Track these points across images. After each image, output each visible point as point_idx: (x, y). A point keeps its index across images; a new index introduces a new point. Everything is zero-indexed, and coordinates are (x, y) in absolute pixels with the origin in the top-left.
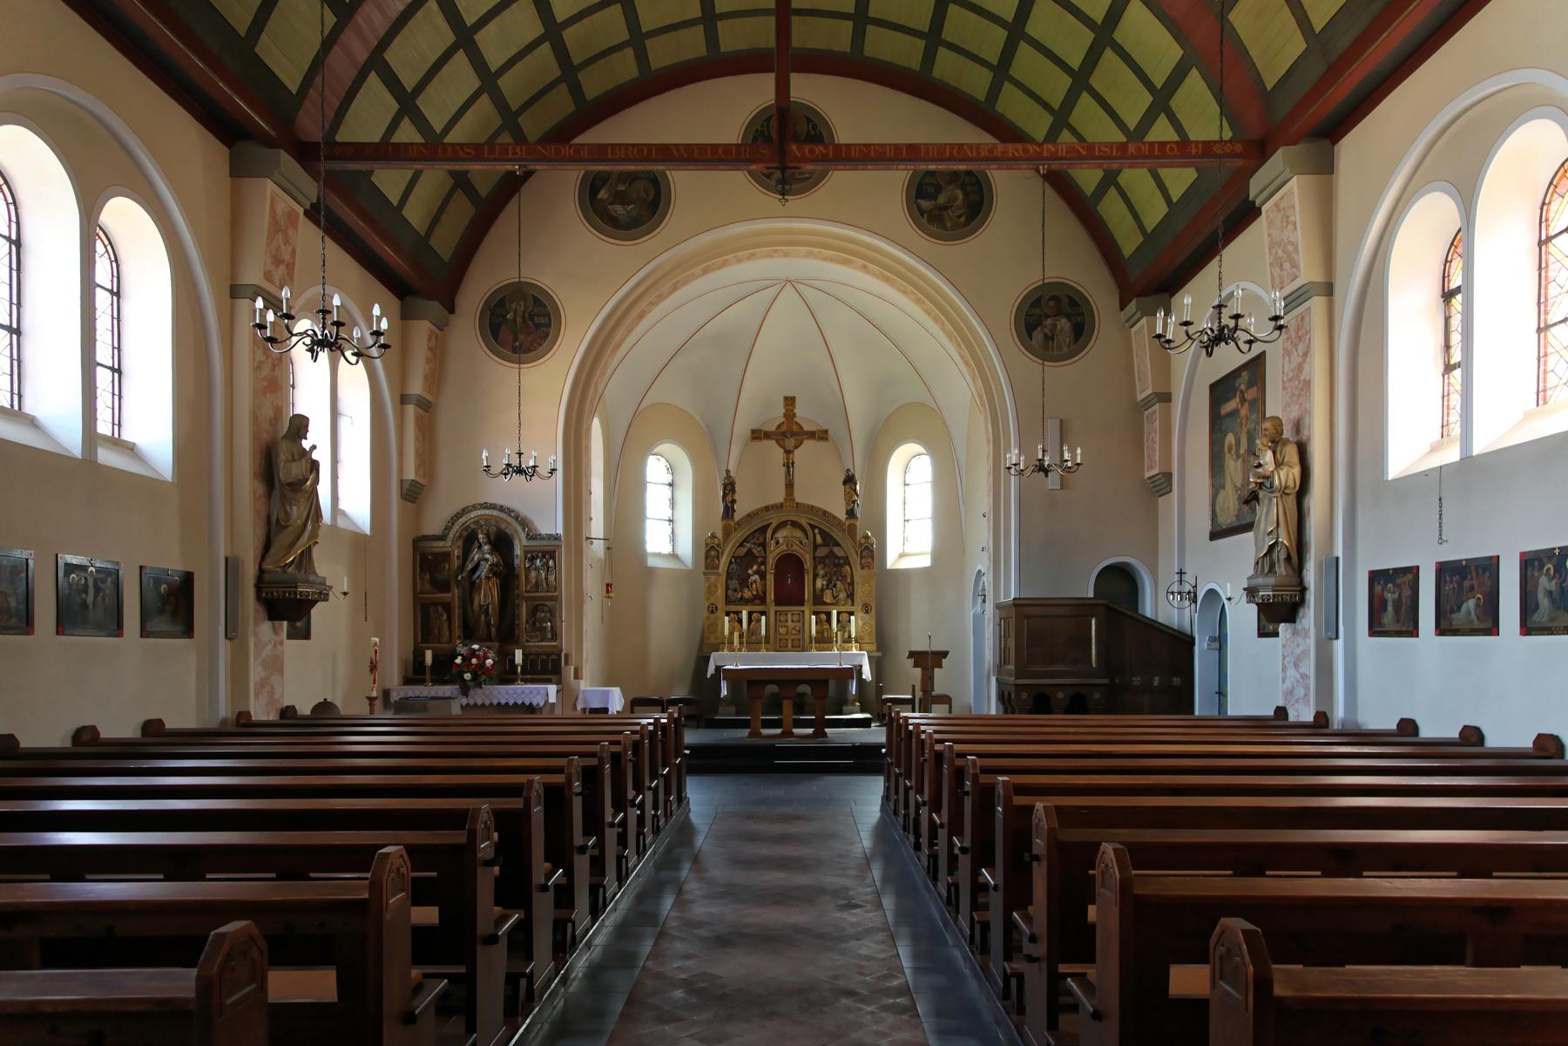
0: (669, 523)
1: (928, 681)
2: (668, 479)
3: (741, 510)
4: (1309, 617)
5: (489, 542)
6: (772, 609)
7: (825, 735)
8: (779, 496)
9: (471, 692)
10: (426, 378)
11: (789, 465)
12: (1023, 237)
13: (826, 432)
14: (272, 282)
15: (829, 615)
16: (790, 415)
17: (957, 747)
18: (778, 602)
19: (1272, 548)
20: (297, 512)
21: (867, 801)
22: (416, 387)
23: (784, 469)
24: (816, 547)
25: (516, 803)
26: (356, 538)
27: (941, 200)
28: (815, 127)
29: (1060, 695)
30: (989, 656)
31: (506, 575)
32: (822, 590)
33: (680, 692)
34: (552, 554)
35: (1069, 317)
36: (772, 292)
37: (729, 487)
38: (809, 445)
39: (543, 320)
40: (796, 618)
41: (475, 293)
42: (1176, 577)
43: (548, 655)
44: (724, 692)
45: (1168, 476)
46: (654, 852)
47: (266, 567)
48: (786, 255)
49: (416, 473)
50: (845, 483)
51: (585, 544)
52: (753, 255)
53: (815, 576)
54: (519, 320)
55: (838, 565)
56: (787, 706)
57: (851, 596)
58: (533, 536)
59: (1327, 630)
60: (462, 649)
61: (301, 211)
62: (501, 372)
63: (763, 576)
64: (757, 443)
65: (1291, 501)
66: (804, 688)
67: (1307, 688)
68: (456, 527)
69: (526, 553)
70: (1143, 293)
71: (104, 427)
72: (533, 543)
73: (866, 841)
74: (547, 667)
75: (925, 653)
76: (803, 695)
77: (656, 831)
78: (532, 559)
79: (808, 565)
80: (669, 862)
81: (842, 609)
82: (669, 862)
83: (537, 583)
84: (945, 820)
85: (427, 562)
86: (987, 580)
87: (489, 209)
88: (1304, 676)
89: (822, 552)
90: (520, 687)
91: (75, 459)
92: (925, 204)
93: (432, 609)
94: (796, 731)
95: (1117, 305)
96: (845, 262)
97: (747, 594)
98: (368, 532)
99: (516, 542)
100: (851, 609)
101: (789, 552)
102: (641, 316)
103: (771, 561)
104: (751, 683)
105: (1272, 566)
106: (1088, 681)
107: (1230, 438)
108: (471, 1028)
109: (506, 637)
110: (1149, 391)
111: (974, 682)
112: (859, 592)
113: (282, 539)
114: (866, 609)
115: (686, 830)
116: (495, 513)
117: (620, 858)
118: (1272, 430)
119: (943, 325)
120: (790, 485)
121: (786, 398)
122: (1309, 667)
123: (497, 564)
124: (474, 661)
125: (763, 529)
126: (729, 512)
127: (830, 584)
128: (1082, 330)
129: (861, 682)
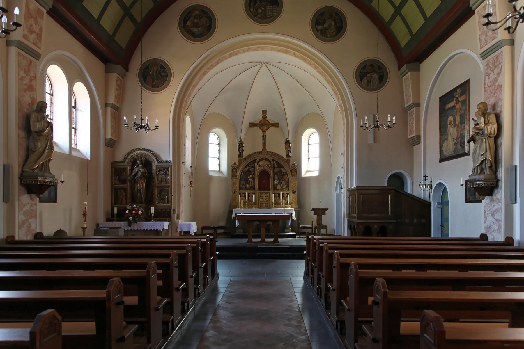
0: (218, 158)
1: (320, 220)
2: (218, 142)
3: (246, 154)
4: (501, 194)
5: (142, 163)
6: (258, 192)
7: (278, 242)
8: (260, 148)
9: (133, 225)
10: (116, 97)
11: (264, 136)
12: (359, 42)
13: (278, 124)
14: (29, 41)
15: (279, 194)
16: (264, 117)
17: (320, 240)
18: (260, 189)
19: (482, 162)
20: (40, 145)
21: (297, 274)
22: (112, 100)
23: (262, 138)
24: (274, 168)
25: (141, 273)
26: (83, 161)
27: (326, 26)
29: (376, 227)
30: (343, 210)
31: (149, 177)
32: (277, 185)
33: (222, 224)
34: (167, 169)
36: (257, 68)
37: (241, 145)
38: (272, 129)
39: (164, 74)
40: (266, 195)
41: (136, 65)
42: (422, 178)
43: (166, 209)
44: (238, 224)
45: (419, 137)
46: (194, 308)
47: (25, 169)
49: (112, 135)
50: (285, 143)
51: (181, 165)
52: (249, 49)
53: (274, 179)
54: (155, 74)
55: (284, 175)
56: (263, 230)
57: (288, 187)
58: (160, 161)
59: (511, 200)
60: (129, 207)
61: (45, 11)
62: (147, 94)
63: (254, 179)
64: (252, 128)
65: (492, 140)
66: (270, 223)
67: (500, 226)
68: (129, 158)
69: (157, 168)
70: (409, 62)
71: (74, 146)
72: (160, 164)
73: (299, 300)
74: (166, 214)
75: (319, 209)
76: (269, 225)
77: (197, 295)
78: (160, 171)
79: (271, 175)
80: (200, 317)
81: (285, 192)
82: (200, 317)
83: (161, 181)
84: (317, 265)
85: (117, 171)
86: (343, 181)
88: (498, 221)
89: (277, 170)
90: (153, 222)
91: (67, 154)
92: (319, 27)
93: (119, 191)
94: (266, 240)
96: (286, 52)
97: (248, 186)
98: (89, 158)
99: (153, 164)
100: (288, 192)
101: (265, 168)
102: (205, 74)
103: (257, 173)
104: (248, 221)
105: (482, 170)
106: (387, 221)
107: (451, 118)
108: (149, 342)
109: (149, 202)
110: (411, 102)
111: (338, 222)
112: (291, 185)
113: (33, 157)
114: (294, 192)
115: (215, 290)
116: (144, 152)
117: (204, 279)
118: (483, 108)
119: (326, 77)
120: (264, 144)
121: (263, 111)
122: (501, 216)
123: (145, 173)
124: (134, 212)
125: (254, 161)
126: (241, 154)
127: (280, 182)
128: (382, 79)
129: (292, 220)
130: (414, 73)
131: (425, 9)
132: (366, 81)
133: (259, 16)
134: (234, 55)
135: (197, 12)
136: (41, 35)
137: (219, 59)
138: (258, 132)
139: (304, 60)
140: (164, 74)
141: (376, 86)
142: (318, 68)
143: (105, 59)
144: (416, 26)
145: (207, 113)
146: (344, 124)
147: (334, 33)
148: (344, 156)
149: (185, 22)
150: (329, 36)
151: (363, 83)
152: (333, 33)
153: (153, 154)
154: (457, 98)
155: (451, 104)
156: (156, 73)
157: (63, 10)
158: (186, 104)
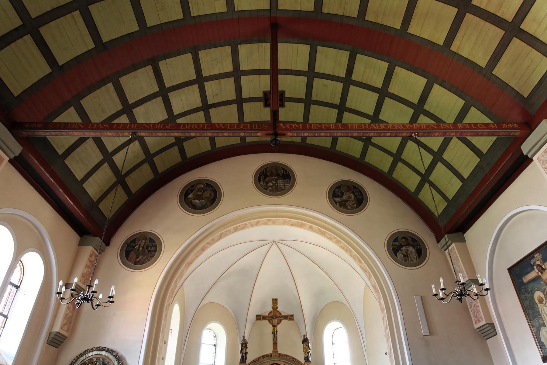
10: (83, 276)
11: (275, 333)
12: (384, 214)
13: (293, 316)
16: (275, 307)
23: (272, 335)
27: (344, 198)
28: (286, 171)
35: (413, 246)
36: (267, 247)
37: (244, 345)
38: (284, 322)
39: (153, 249)
45: (492, 325)
48: (274, 223)
50: (303, 342)
52: (258, 222)
54: (141, 249)
62: (125, 272)
64: (259, 322)
87: (135, 201)
92: (337, 199)
95: (435, 241)
96: (301, 226)
102: (203, 249)
116: (103, 353)
120: (275, 344)
121: (273, 300)
128: (421, 253)
130: (459, 244)
131: (460, 171)
132: (401, 255)
133: (270, 188)
134: (240, 230)
135: (202, 186)
137: (222, 233)
138: (267, 326)
139: (322, 233)
140: (153, 249)
142: (340, 242)
145: (204, 302)
146: (382, 310)
147: (355, 205)
148: (390, 356)
149: (187, 194)
150: (349, 207)
151: (398, 258)
153: (116, 357)
154: (538, 265)
155: (532, 275)
156: (143, 247)
158: (176, 286)
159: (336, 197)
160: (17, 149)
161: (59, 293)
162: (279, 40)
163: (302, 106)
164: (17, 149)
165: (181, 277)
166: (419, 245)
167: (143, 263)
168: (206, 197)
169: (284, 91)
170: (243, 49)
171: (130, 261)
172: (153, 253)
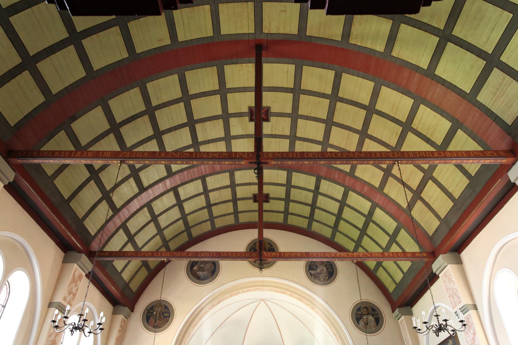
12: (350, 286)
27: (318, 270)
28: (271, 246)
35: (373, 315)
36: (257, 303)
39: (167, 315)
52: (249, 290)
61: (84, 274)
70: (400, 307)
87: (153, 274)
96: (284, 293)
128: (378, 321)
136: (76, 294)
140: (167, 315)
141: (373, 328)
143: (114, 301)
144: (399, 276)
151: (360, 325)
152: (325, 277)
156: (160, 313)
157: (25, 184)
159: (311, 270)
160: (11, 175)
161: (54, 321)
162: (263, 59)
163: (288, 120)
164: (11, 175)
165: (188, 337)
166: (378, 314)
167: (160, 327)
168: (208, 270)
169: (270, 107)
170: (229, 69)
171: (150, 325)
172: (167, 318)
